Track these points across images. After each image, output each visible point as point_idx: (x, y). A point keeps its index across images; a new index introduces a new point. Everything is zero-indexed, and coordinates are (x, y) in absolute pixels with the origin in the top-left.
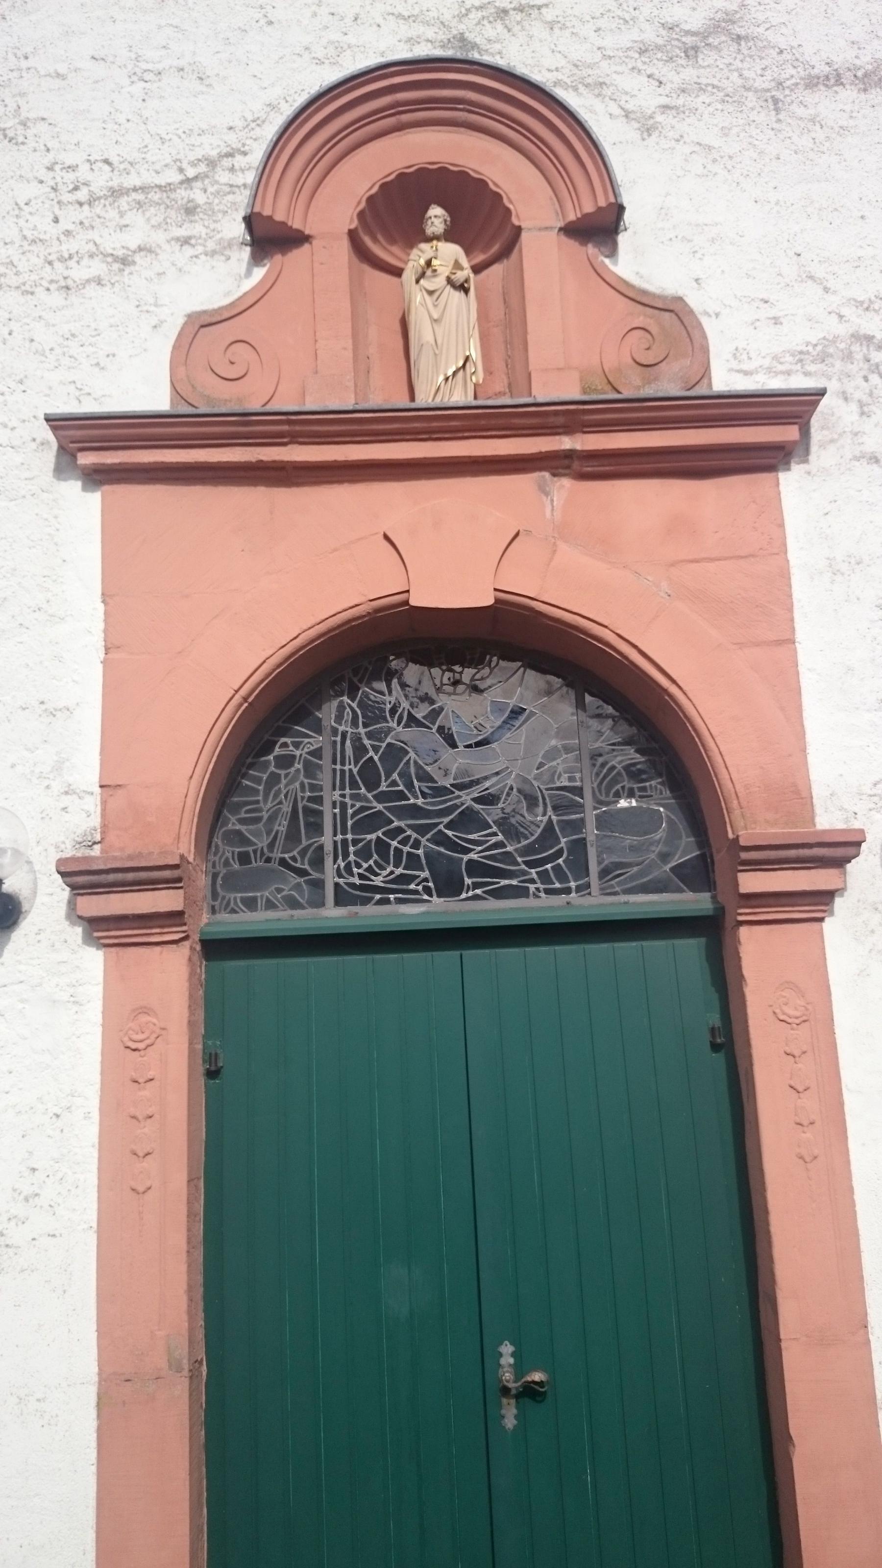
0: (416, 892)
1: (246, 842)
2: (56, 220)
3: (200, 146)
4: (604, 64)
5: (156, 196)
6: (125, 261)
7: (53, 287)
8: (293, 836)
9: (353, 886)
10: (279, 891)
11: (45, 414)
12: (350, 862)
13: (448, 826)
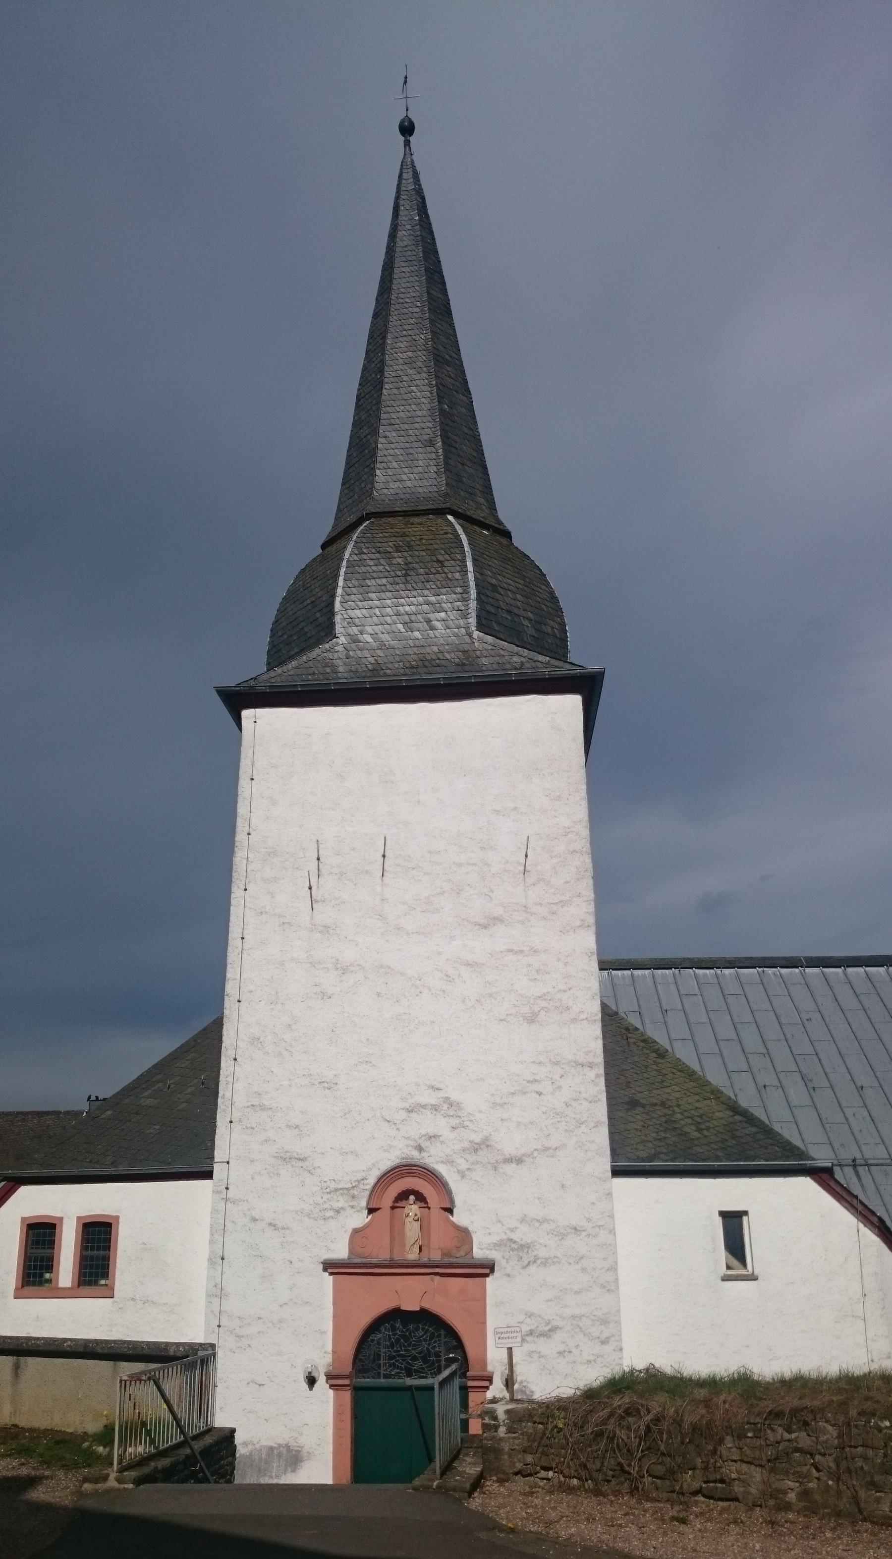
1: (363, 1362)
2: (322, 1198)
4: (454, 1155)
5: (345, 1192)
6: (338, 1212)
8: (374, 1361)
13: (410, 1360)
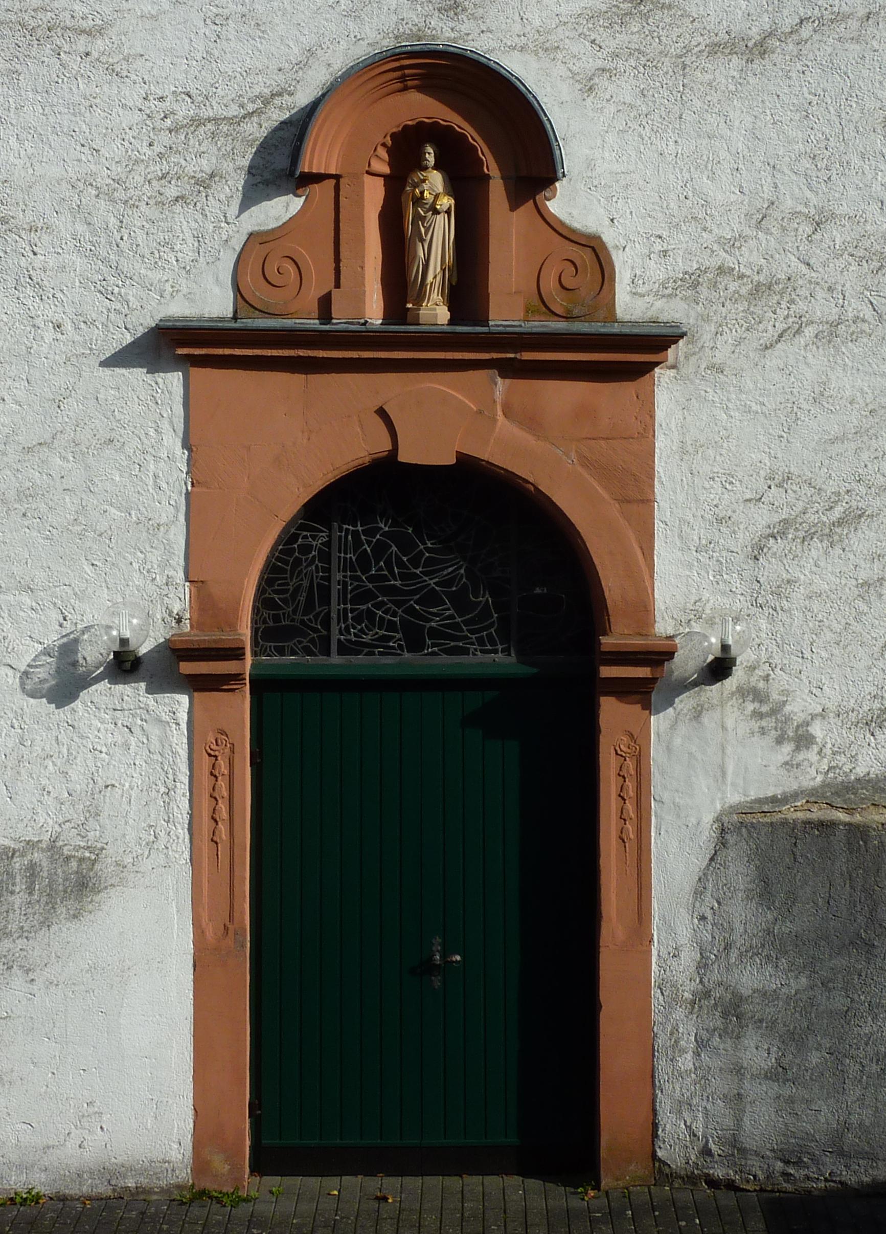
0: (393, 648)
3: (257, 84)
7: (152, 202)
8: (309, 606)
9: (349, 641)
10: (300, 642)
12: (348, 625)
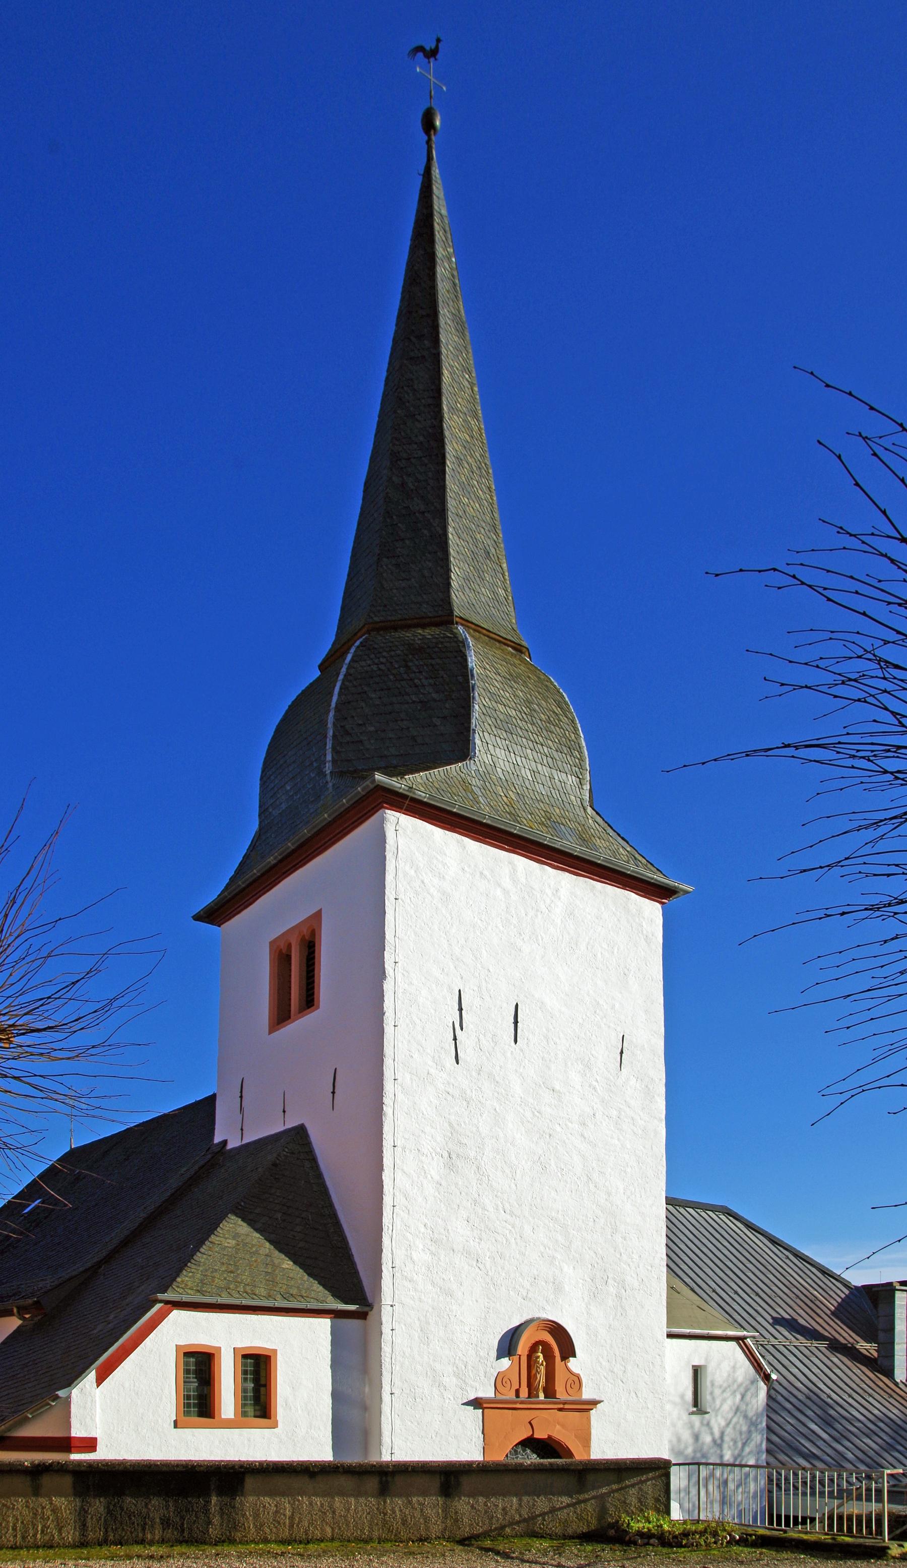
11: (275, 1426)
